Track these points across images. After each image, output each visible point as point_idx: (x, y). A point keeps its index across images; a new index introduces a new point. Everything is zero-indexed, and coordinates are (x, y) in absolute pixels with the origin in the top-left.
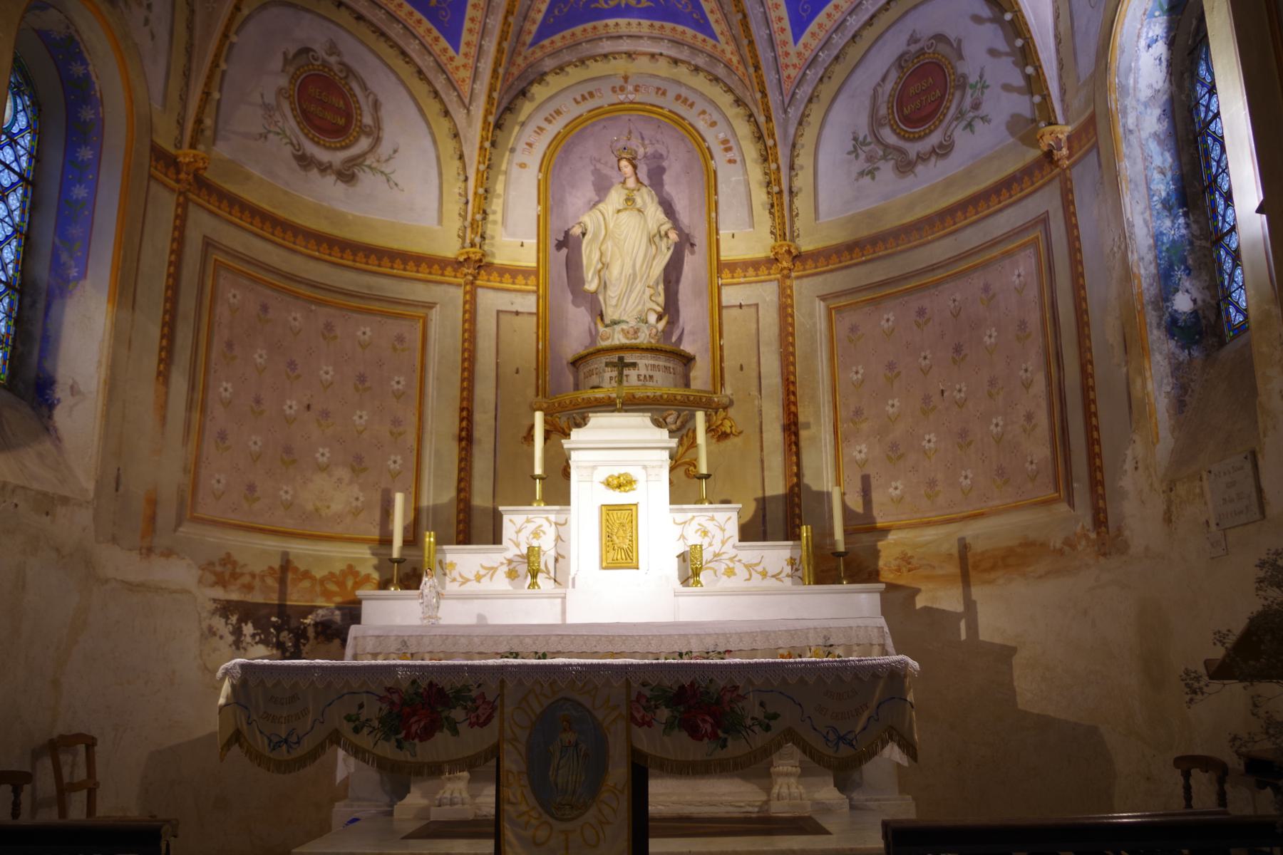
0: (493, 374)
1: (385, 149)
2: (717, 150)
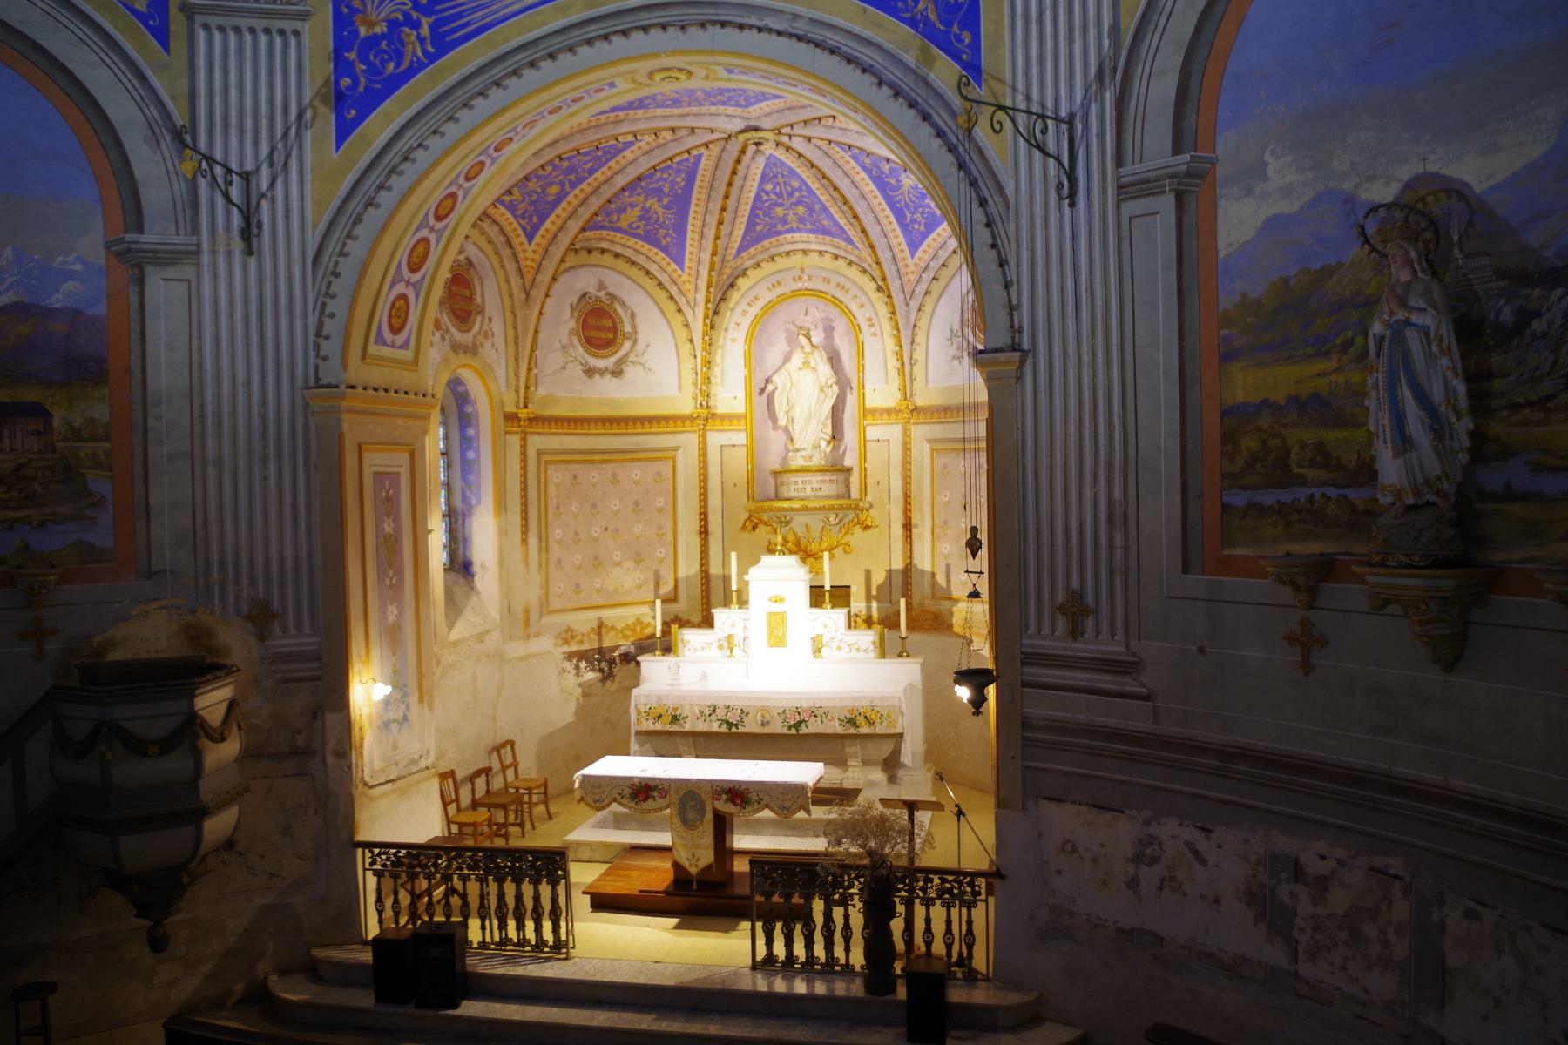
0: (720, 488)
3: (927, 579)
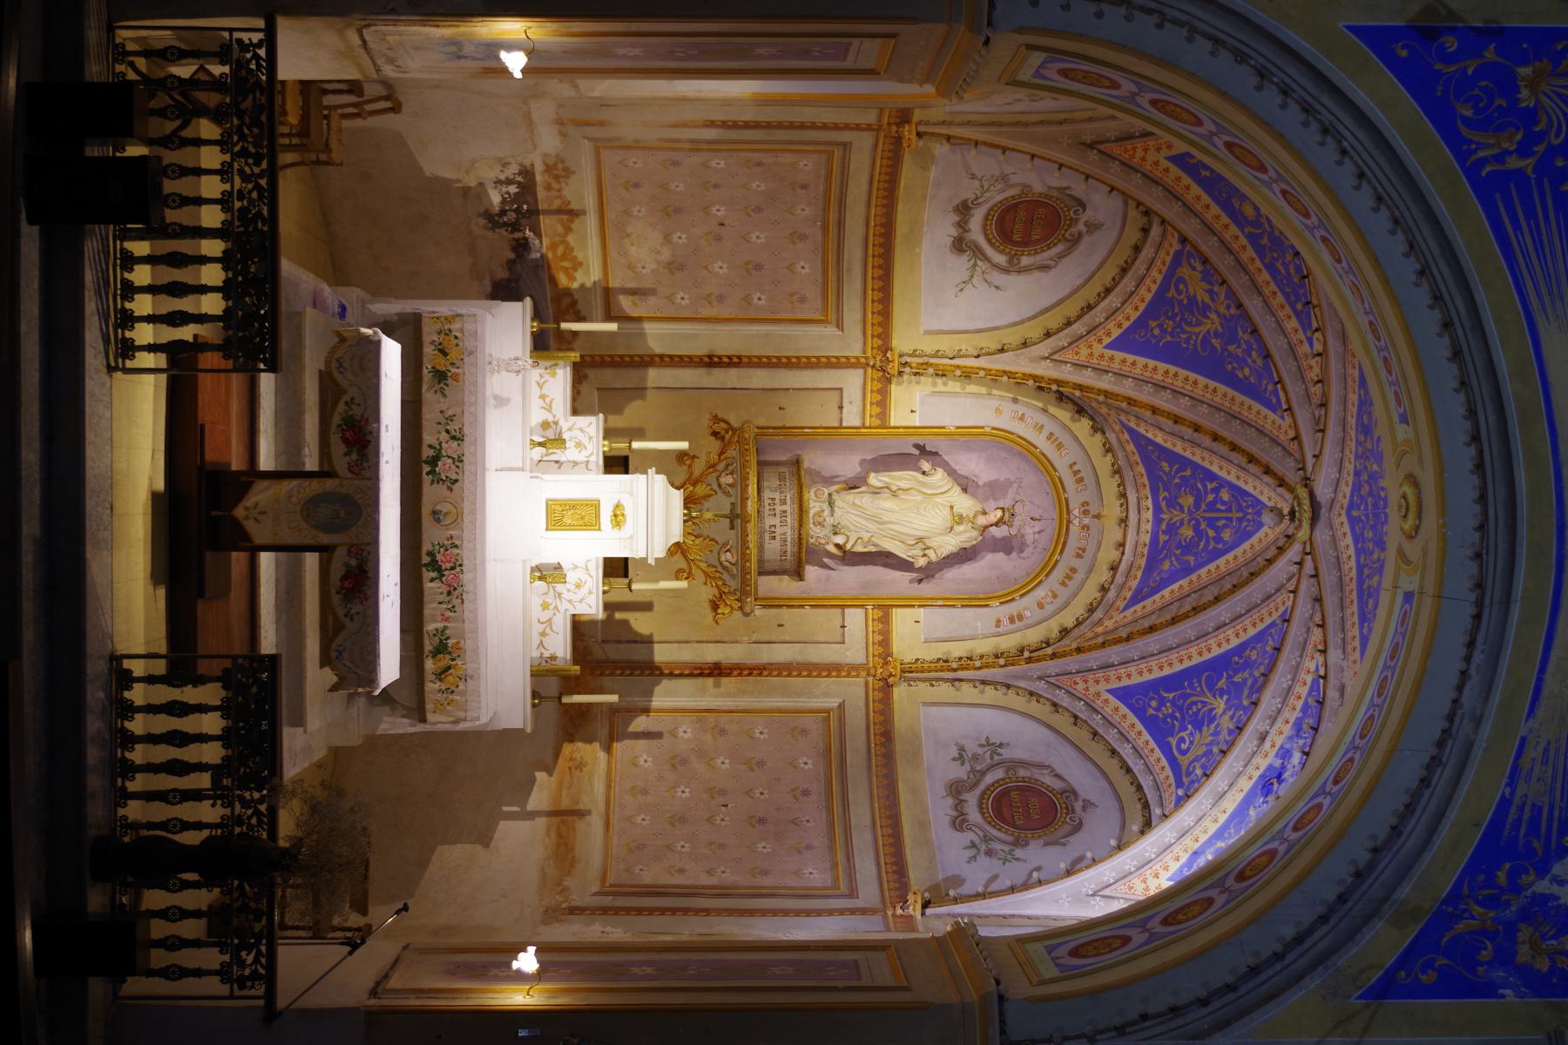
1: (998, 278)
2: (1012, 608)
3: (639, 701)
